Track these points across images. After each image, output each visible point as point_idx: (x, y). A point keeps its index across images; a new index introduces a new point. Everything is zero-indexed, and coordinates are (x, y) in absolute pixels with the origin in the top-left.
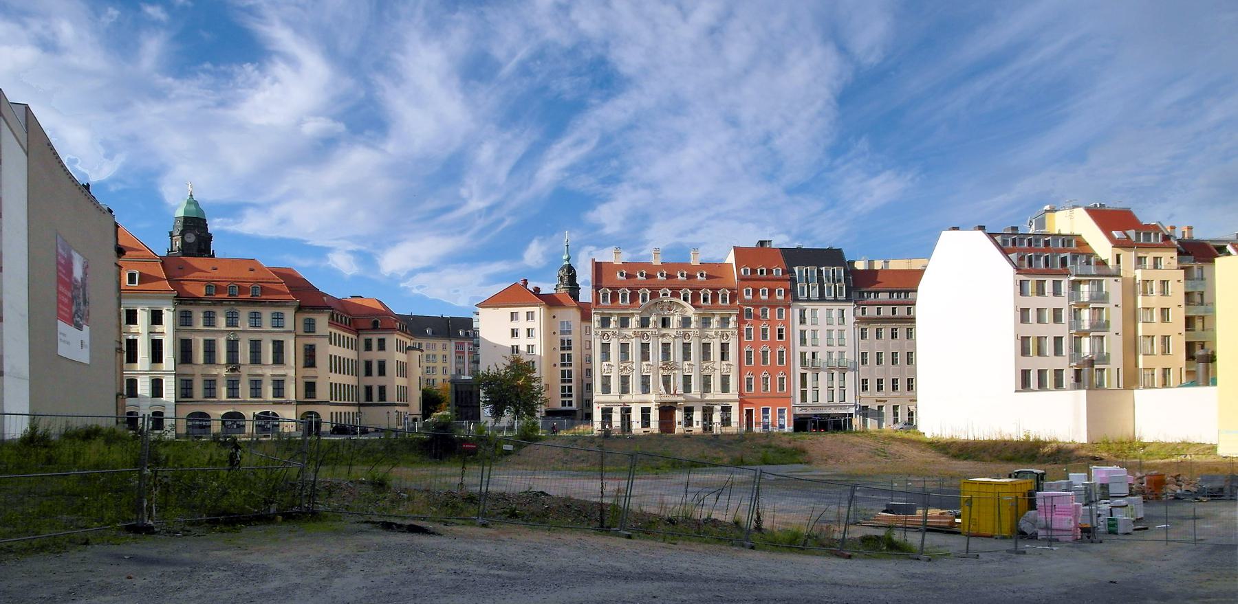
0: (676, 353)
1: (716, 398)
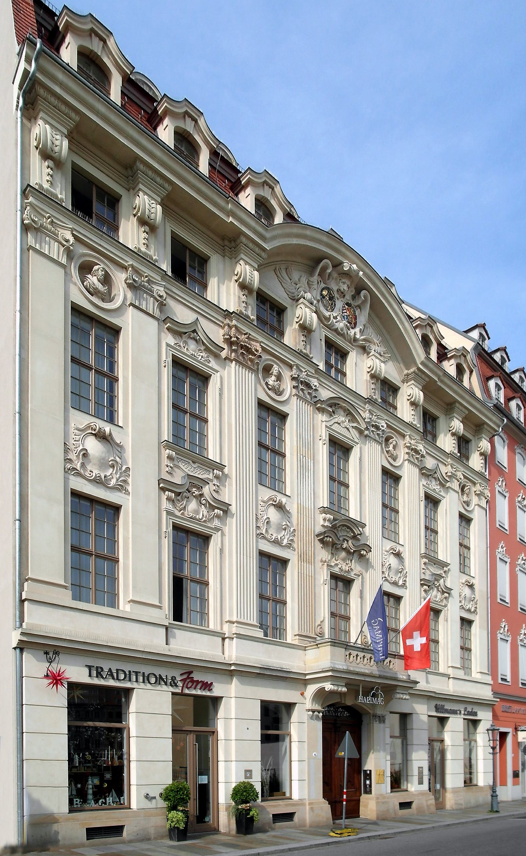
1: (234, 653)
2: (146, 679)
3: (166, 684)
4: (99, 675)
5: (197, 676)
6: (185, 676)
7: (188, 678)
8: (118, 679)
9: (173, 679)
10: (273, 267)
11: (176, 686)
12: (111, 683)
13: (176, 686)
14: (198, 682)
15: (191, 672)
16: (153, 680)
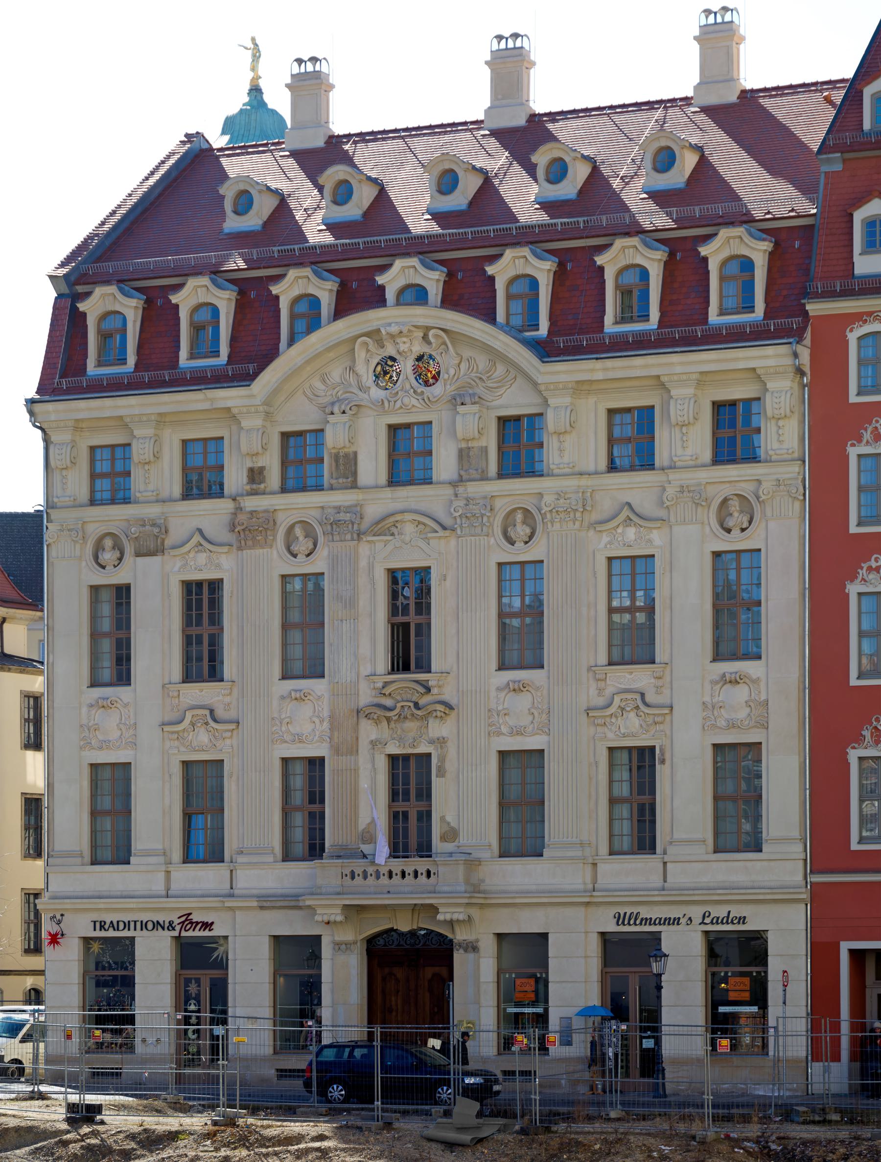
0: (462, 633)
2: (144, 926)
3: (163, 928)
4: (102, 927)
5: (195, 918)
6: (183, 919)
7: (186, 920)
8: (118, 930)
9: (171, 923)
11: (174, 929)
12: (111, 933)
13: (174, 929)
14: (197, 923)
15: (190, 914)
16: (150, 926)
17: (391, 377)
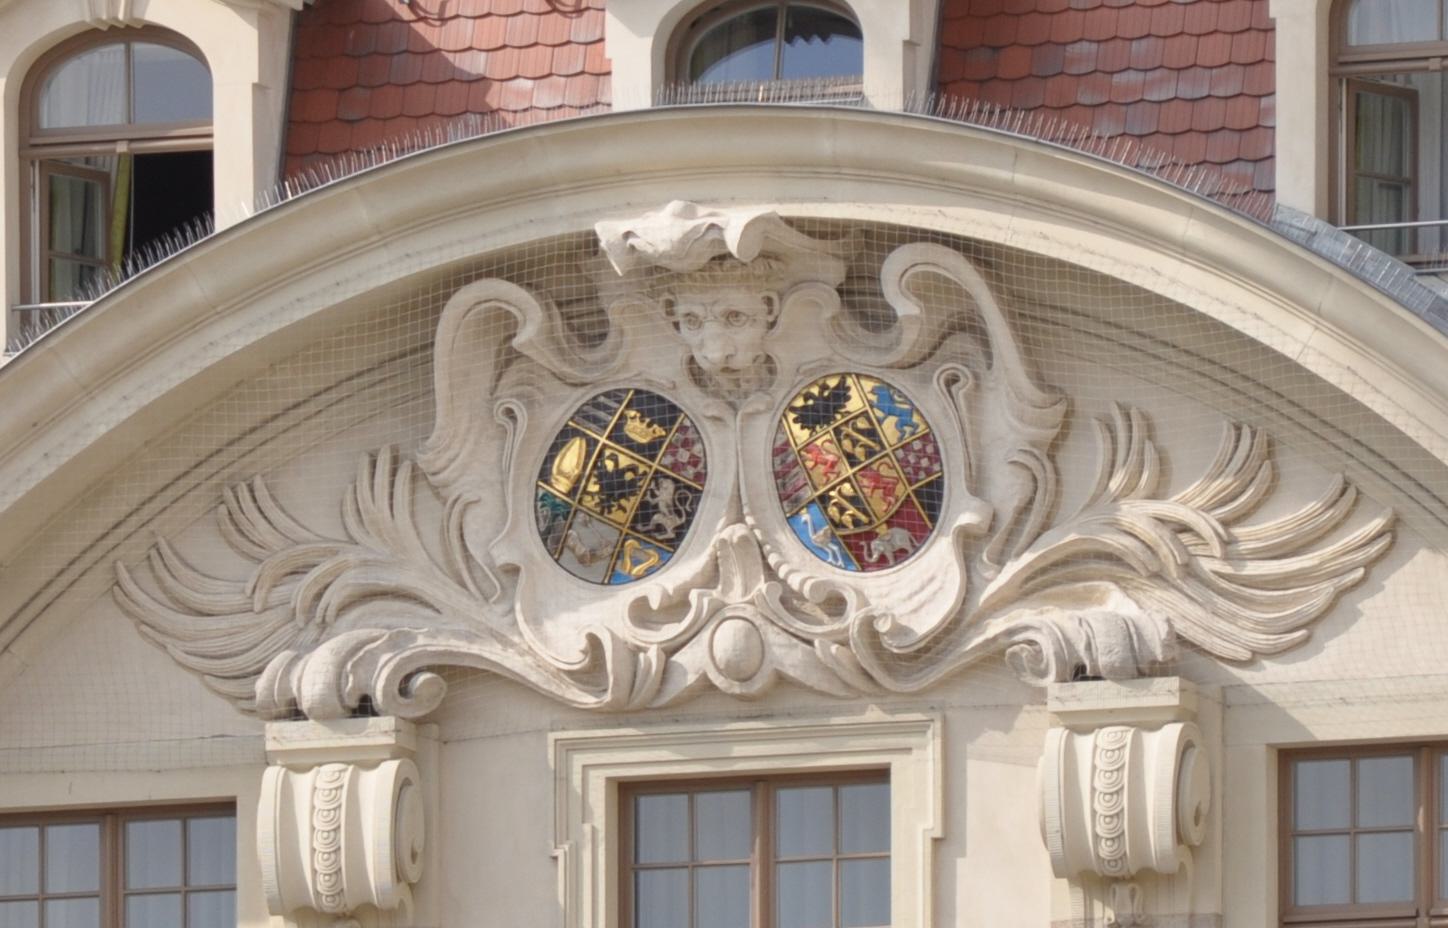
10: (98, 580)
17: (646, 511)
